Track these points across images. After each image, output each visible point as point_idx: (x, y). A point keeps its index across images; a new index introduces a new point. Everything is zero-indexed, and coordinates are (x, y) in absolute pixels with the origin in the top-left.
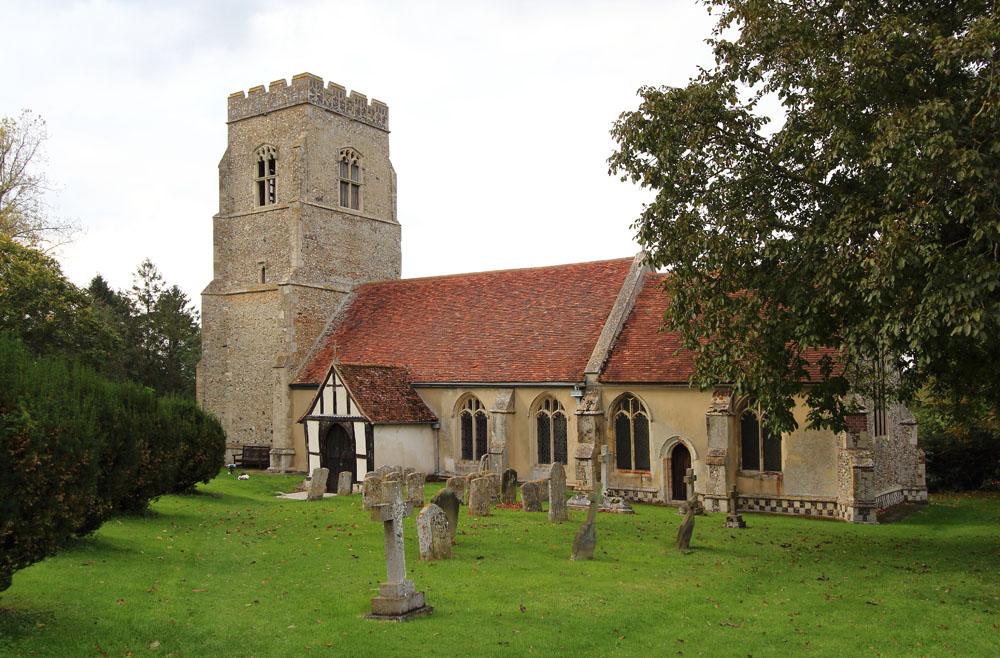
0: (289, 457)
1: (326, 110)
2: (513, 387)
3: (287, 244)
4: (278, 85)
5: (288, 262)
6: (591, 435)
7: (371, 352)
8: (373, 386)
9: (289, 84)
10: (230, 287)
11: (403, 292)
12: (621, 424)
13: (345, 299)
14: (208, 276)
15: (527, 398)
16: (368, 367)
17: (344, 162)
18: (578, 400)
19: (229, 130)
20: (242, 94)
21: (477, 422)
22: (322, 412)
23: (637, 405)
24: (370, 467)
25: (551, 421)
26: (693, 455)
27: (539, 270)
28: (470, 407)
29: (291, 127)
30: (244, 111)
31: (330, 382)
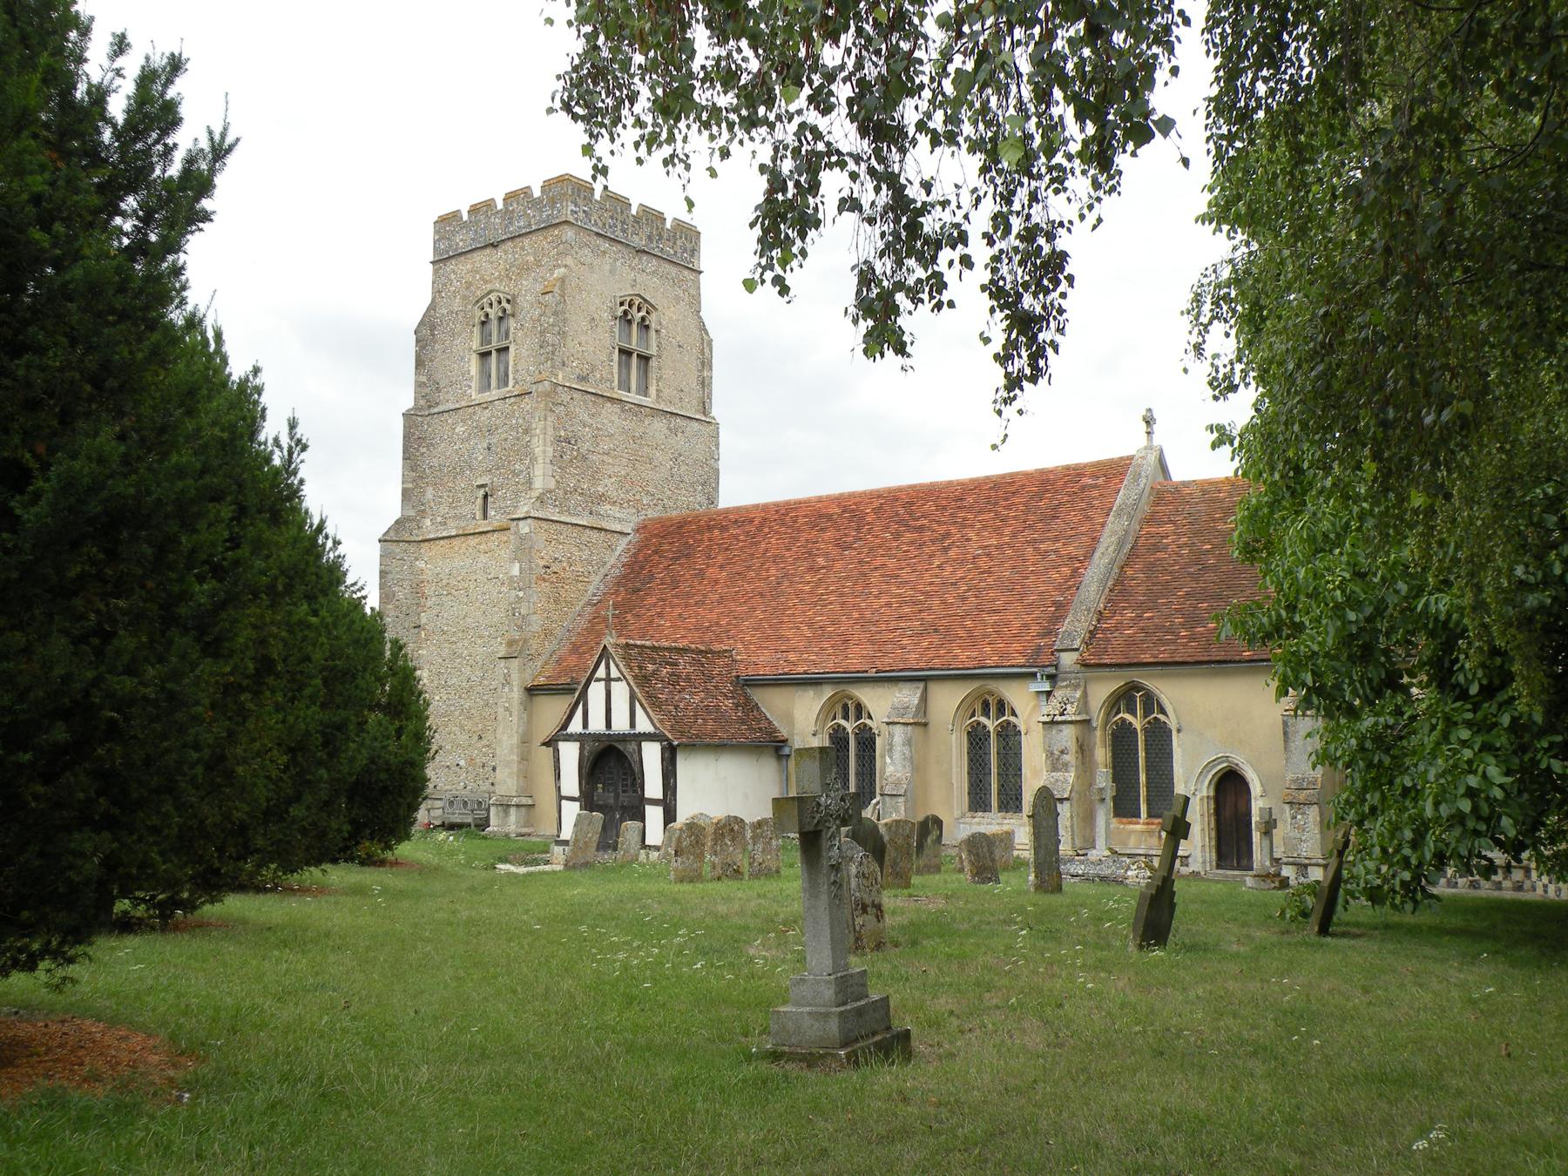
0: (523, 810)
1: (598, 234)
2: (925, 679)
3: (526, 452)
4: (518, 196)
5: (529, 482)
6: (1066, 758)
7: (671, 630)
8: (674, 680)
9: (537, 193)
10: (428, 527)
11: (724, 529)
12: (1122, 739)
13: (623, 543)
14: (391, 508)
15: (948, 701)
16: (669, 649)
17: (626, 319)
18: (1044, 698)
19: (435, 272)
20: (456, 215)
21: (858, 743)
22: (585, 725)
23: (1151, 703)
24: (670, 816)
25: (1141, 738)
26: (1256, 788)
27: (961, 483)
28: (846, 717)
29: (538, 263)
30: (462, 241)
31: (601, 672)
